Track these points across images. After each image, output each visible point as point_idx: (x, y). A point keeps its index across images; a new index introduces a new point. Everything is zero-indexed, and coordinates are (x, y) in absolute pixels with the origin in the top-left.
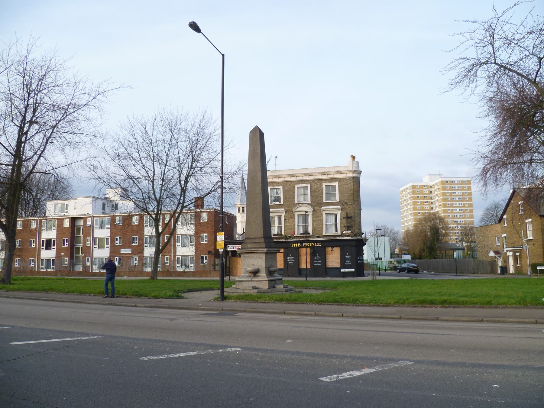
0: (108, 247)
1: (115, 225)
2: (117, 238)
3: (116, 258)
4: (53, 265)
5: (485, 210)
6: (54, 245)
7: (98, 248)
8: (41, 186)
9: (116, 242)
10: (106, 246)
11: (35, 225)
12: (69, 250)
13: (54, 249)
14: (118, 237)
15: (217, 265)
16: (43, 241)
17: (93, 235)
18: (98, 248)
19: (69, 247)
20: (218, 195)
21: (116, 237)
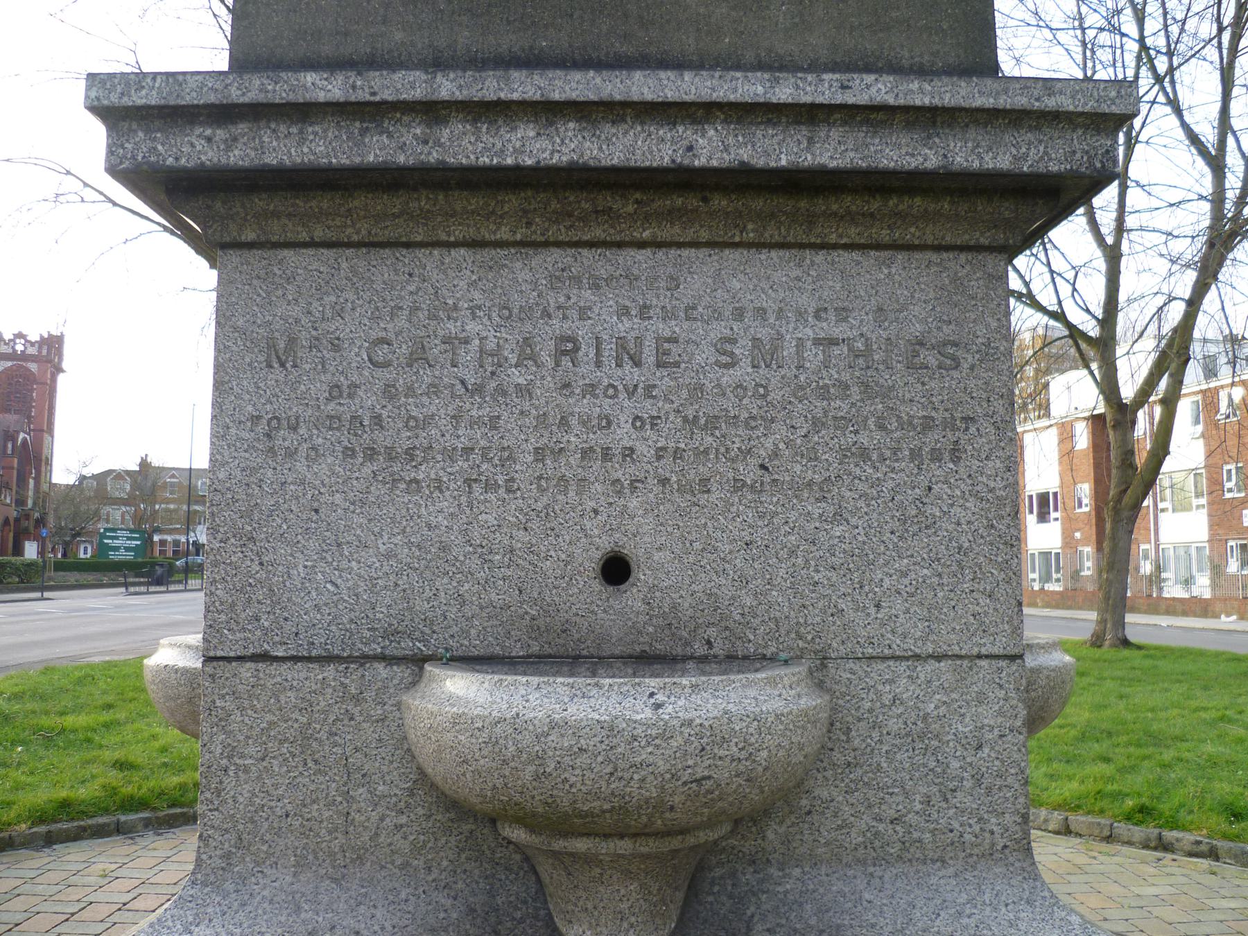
0: (1203, 506)
1: (1216, 424)
2: (1229, 471)
3: (1232, 547)
4: (1058, 571)
5: (46, 336)
6: (1056, 509)
7: (1174, 511)
8: (585, 866)
9: (1228, 485)
10: (1195, 502)
11: (901, 654)
12: (1094, 521)
13: (1056, 519)
14: (1232, 467)
15: (1061, 94)
16: (1031, 497)
17: (1157, 540)
18: (1174, 511)
19: (1093, 513)
20: (1232, 182)
21: (1226, 467)
